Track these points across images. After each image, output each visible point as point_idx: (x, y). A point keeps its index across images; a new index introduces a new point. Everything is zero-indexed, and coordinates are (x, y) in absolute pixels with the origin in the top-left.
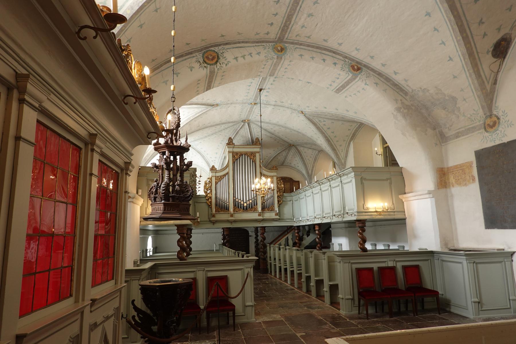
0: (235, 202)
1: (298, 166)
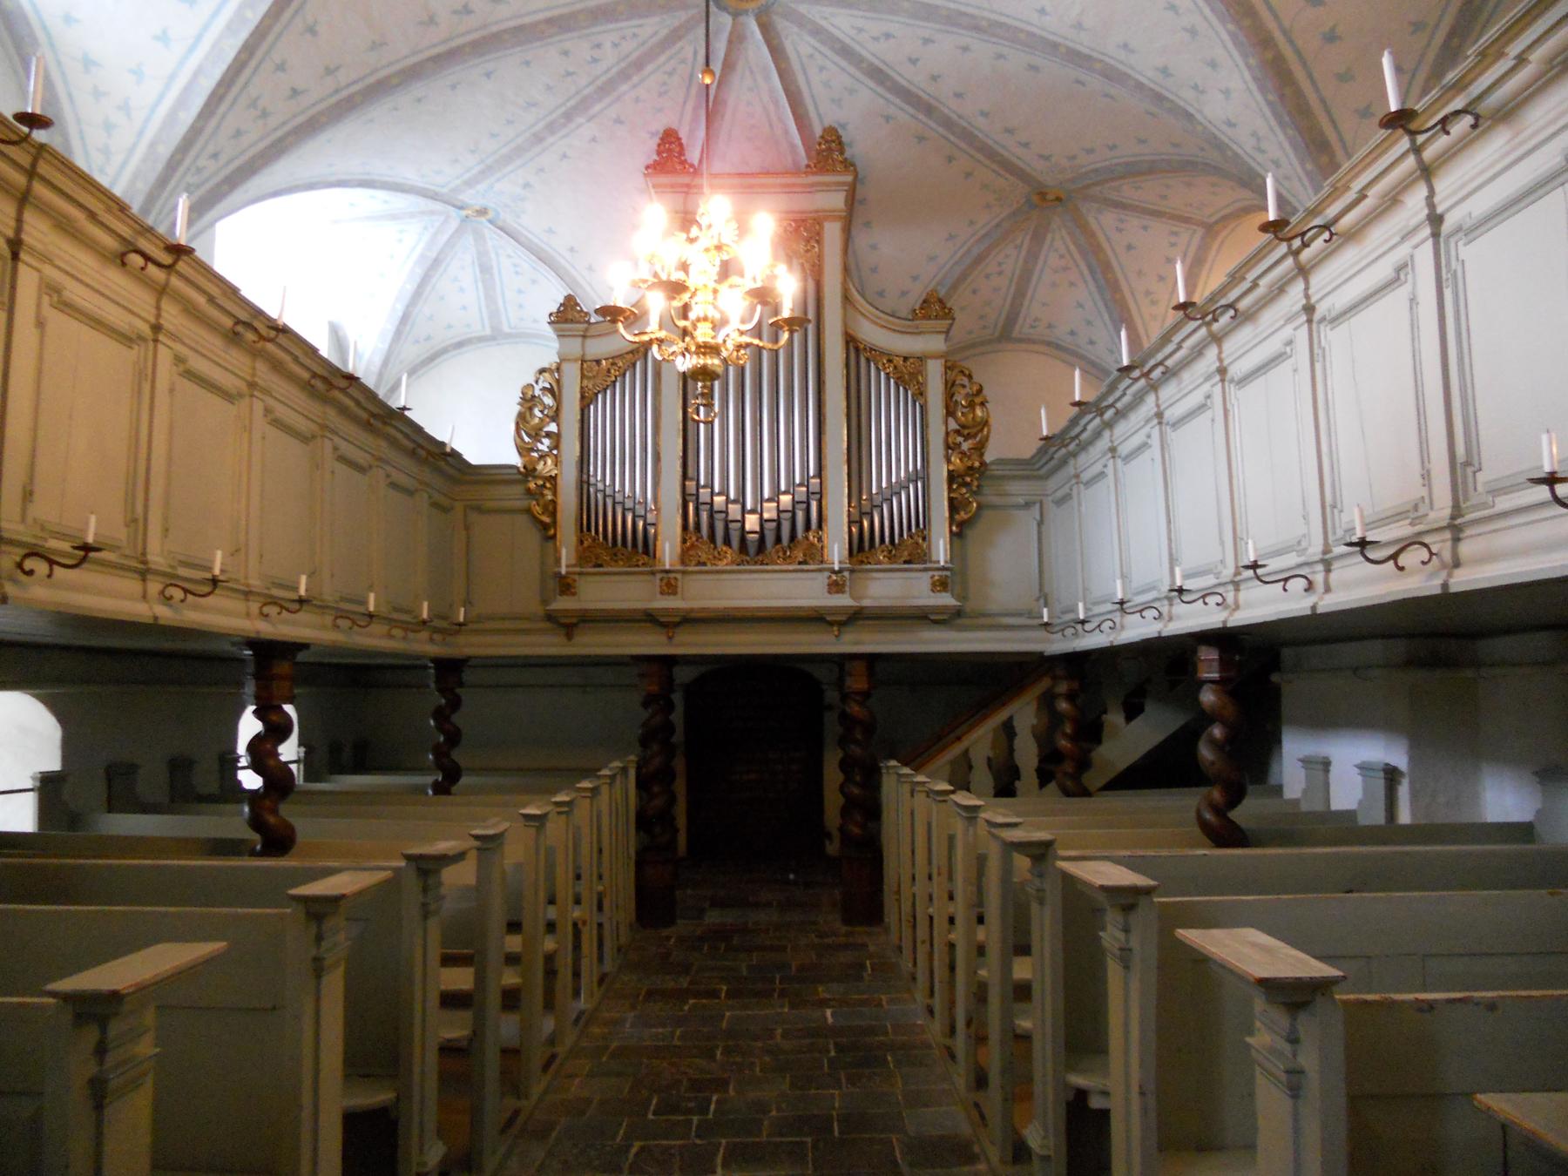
0: (585, 486)
1: (1092, 342)
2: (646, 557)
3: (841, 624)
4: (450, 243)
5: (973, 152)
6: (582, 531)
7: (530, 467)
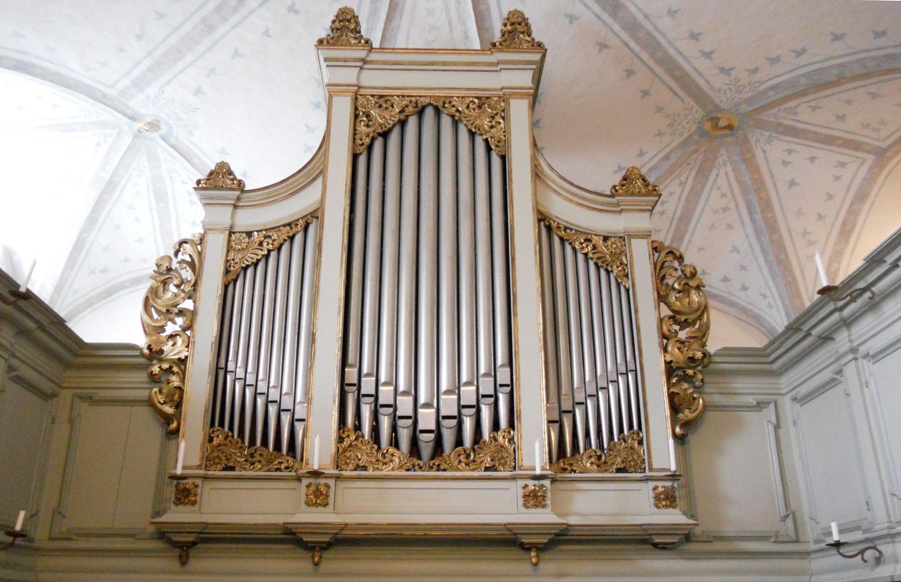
0: (221, 373)
1: (744, 288)
2: (291, 460)
3: (541, 549)
6: (212, 424)
7: (154, 348)
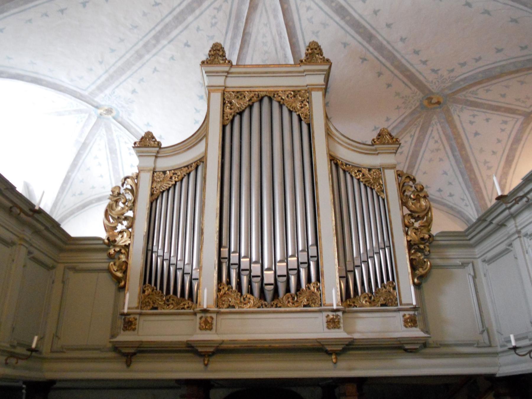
1: (451, 195)
2: (190, 303)
3: (338, 353)
4: (92, 133)
5: (392, 68)
7: (111, 239)
